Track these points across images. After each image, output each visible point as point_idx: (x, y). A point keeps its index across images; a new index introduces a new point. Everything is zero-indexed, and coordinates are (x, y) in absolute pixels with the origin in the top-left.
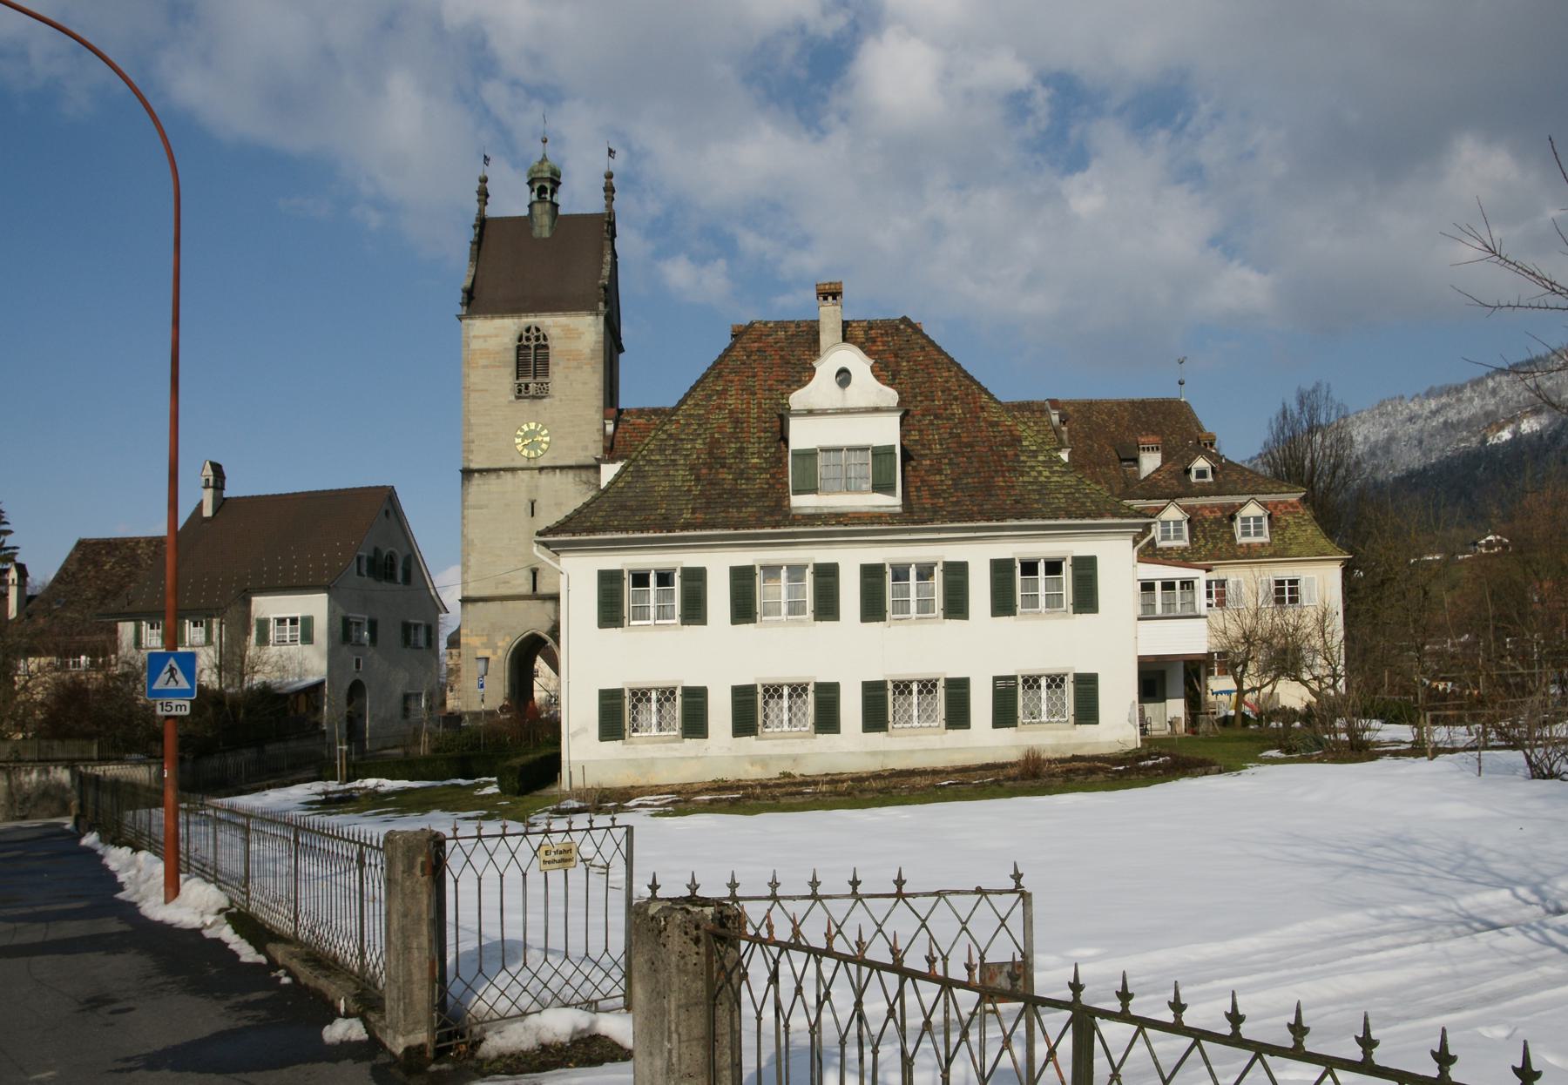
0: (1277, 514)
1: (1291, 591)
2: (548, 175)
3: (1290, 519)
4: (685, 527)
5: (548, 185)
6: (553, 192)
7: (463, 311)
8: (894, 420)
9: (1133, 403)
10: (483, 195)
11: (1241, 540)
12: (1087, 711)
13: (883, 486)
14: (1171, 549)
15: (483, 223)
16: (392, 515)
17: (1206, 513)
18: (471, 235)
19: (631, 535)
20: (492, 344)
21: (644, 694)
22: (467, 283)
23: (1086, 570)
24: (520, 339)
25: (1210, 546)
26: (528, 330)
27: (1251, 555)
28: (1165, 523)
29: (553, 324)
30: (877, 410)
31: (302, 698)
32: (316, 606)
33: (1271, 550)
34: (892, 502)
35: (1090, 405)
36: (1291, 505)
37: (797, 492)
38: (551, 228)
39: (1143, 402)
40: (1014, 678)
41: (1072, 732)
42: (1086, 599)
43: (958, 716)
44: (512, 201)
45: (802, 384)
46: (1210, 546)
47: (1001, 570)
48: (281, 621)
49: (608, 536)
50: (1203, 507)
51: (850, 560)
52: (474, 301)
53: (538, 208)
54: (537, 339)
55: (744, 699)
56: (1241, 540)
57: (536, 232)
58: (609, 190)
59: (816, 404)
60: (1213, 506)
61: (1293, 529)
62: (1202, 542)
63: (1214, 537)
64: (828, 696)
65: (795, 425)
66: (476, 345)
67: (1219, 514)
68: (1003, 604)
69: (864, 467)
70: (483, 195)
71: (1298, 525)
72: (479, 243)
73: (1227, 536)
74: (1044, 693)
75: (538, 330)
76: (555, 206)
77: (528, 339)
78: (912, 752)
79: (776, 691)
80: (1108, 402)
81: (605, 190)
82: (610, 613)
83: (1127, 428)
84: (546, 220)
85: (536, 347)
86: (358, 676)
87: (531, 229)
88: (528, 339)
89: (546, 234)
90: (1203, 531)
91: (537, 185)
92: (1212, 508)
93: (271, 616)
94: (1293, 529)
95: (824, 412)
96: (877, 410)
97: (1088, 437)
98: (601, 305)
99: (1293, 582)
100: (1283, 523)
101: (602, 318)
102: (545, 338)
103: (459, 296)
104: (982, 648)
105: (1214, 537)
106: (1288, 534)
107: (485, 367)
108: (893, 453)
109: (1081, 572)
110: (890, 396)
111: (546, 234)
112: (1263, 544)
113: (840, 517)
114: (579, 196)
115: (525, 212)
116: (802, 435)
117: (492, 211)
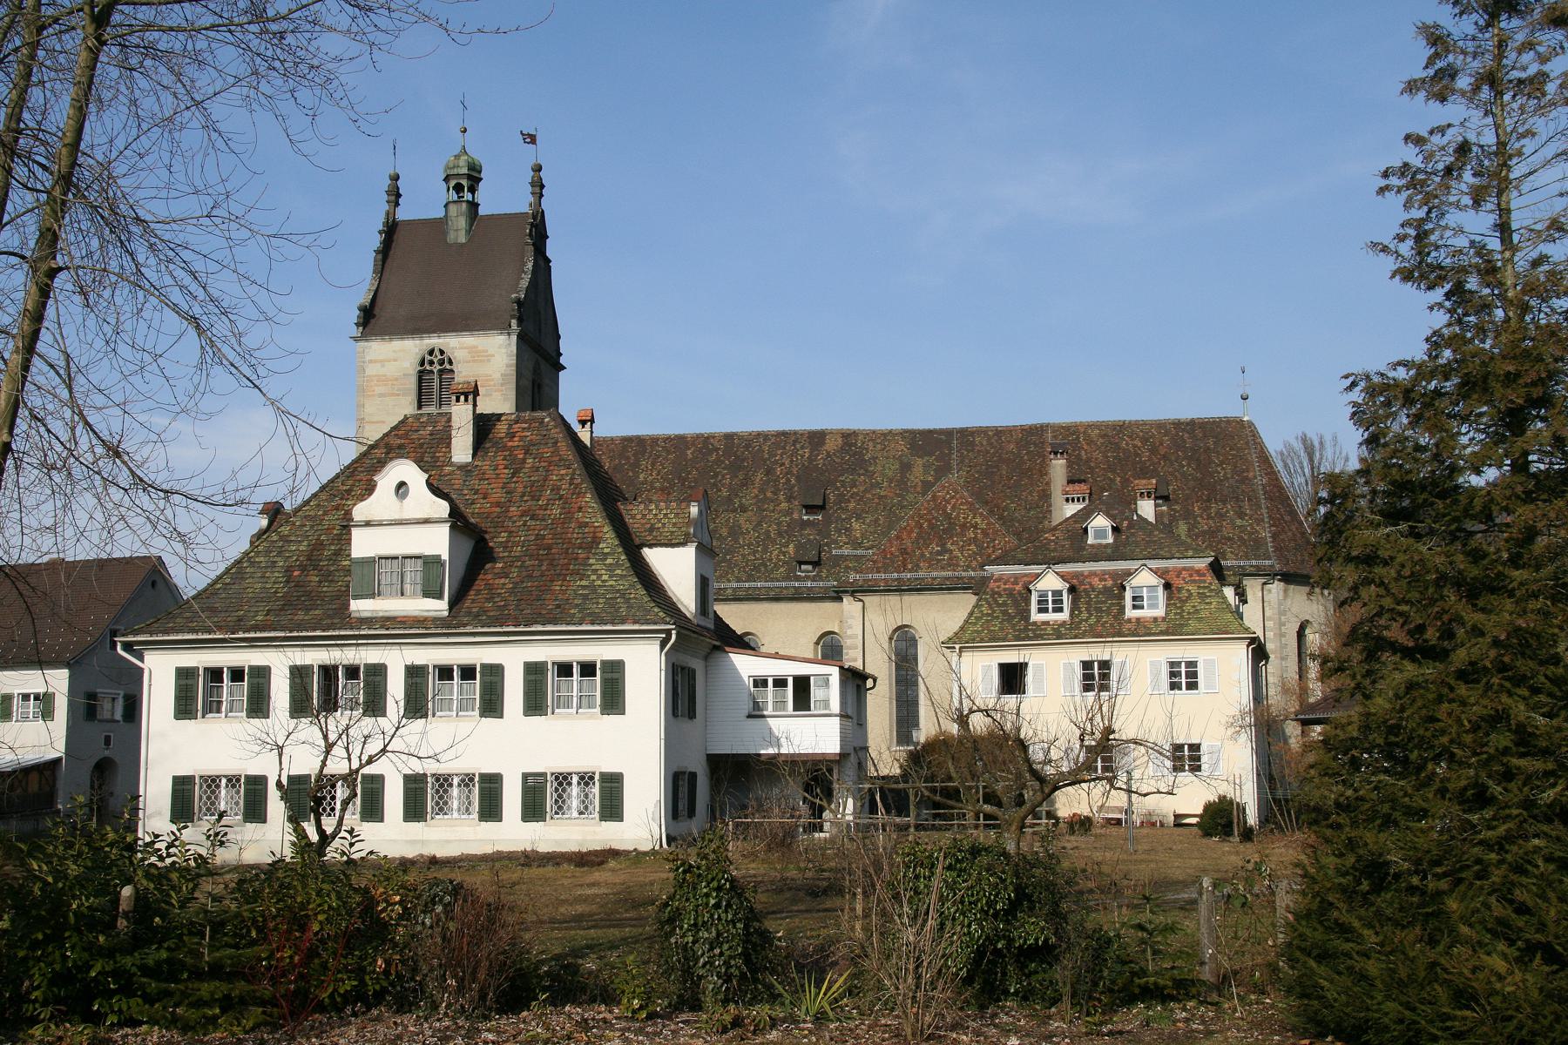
0: (1177, 582)
1: (1188, 675)
2: (465, 171)
3: (1193, 589)
4: (256, 628)
5: (464, 182)
6: (472, 190)
7: (356, 332)
8: (444, 530)
9: (1178, 424)
10: (395, 195)
11: (1036, 617)
12: (612, 808)
13: (432, 592)
14: (1047, 623)
15: (391, 230)
16: (160, 585)
17: (1096, 581)
18: (376, 241)
19: (201, 636)
20: (391, 370)
21: (565, 778)
22: (364, 298)
23: (613, 675)
24: (422, 363)
25: (1093, 620)
26: (431, 352)
27: (1142, 632)
28: (1043, 595)
29: (458, 345)
30: (426, 521)
31: (34, 776)
32: (58, 681)
33: (1163, 626)
34: (439, 607)
35: (1121, 428)
36: (1198, 572)
37: (356, 597)
38: (468, 231)
39: (1192, 422)
40: (544, 775)
41: (598, 829)
42: (613, 701)
43: (491, 809)
44: (426, 200)
45: (362, 498)
46: (1093, 620)
47: (534, 672)
48: (26, 697)
49: (180, 637)
50: (1093, 574)
51: (396, 660)
52: (370, 320)
53: (453, 209)
54: (441, 362)
55: (415, 787)
56: (1036, 617)
57: (451, 237)
58: (538, 186)
59: (376, 516)
60: (1104, 573)
61: (1195, 601)
62: (1085, 615)
63: (1099, 610)
64: (491, 786)
65: (356, 534)
66: (371, 370)
67: (1110, 583)
68: (535, 704)
69: (413, 572)
70: (395, 195)
71: (1202, 596)
72: (385, 252)
73: (1115, 610)
74: (455, 791)
75: (442, 352)
76: (474, 206)
77: (431, 363)
78: (448, 842)
79: (565, 778)
80: (1144, 423)
81: (533, 184)
82: (185, 708)
83: (1164, 457)
84: (462, 223)
85: (441, 372)
86: (107, 753)
87: (445, 233)
88: (431, 363)
89: (462, 239)
90: (1088, 603)
91: (452, 183)
92: (1102, 575)
93: (16, 692)
94: (1195, 601)
95: (380, 524)
96: (426, 521)
97: (1111, 469)
98: (514, 322)
99: (1192, 664)
100: (1184, 594)
101: (514, 338)
102: (451, 362)
103: (354, 315)
104: (514, 745)
105: (1099, 610)
106: (1188, 607)
107: (381, 395)
108: (443, 565)
109: (609, 676)
110: (442, 508)
111: (462, 239)
112: (1155, 619)
113: (388, 621)
114: (502, 196)
115: (442, 214)
116: (363, 544)
117: (402, 214)
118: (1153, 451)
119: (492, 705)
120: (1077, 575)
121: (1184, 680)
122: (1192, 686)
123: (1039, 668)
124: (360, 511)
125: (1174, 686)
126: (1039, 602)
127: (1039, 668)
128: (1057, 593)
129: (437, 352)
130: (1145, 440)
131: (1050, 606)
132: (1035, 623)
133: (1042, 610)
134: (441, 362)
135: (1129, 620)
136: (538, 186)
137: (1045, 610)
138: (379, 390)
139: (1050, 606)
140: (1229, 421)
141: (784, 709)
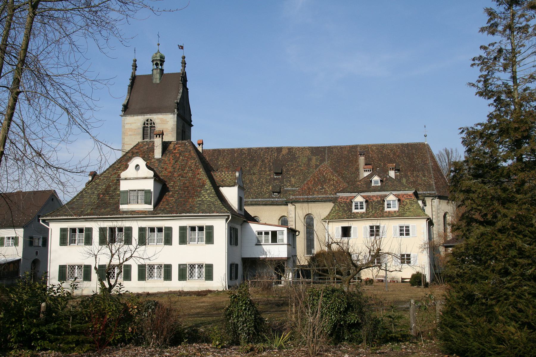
0: (402, 199)
1: (406, 231)
2: (159, 58)
3: (408, 201)
4: (87, 215)
5: (159, 62)
6: (161, 65)
7: (122, 113)
8: (152, 181)
9: (403, 145)
10: (135, 67)
11: (354, 211)
12: (209, 276)
13: (148, 202)
14: (358, 213)
15: (134, 78)
16: (55, 200)
17: (375, 199)
18: (129, 82)
19: (69, 217)
20: (134, 126)
21: (193, 266)
22: (124, 102)
23: (210, 231)
24: (144, 124)
25: (373, 212)
26: (147, 120)
27: (390, 216)
28: (356, 203)
29: (156, 118)
30: (146, 178)
31: (12, 265)
32: (20, 233)
33: (398, 214)
34: (150, 207)
35: (383, 146)
36: (410, 195)
37: (122, 204)
38: (160, 79)
39: (407, 144)
40: (186, 265)
41: (204, 283)
42: (210, 239)
43: (168, 276)
44: (146, 68)
45: (124, 170)
46: (373, 212)
47: (183, 229)
48: (9, 238)
49: (61, 218)
50: (374, 196)
51: (135, 226)
52: (127, 109)
53: (155, 71)
54: (151, 124)
55: (142, 269)
56: (354, 211)
57: (154, 81)
58: (184, 64)
59: (128, 176)
60: (377, 196)
61: (409, 205)
62: (371, 210)
63: (376, 208)
64: (168, 269)
65: (122, 182)
66: (127, 126)
67: (379, 199)
68: (183, 240)
69: (141, 195)
70: (135, 67)
71: (411, 204)
72: (132, 86)
73: (381, 208)
74: (156, 270)
75: (151, 120)
76: (162, 70)
77: (147, 124)
78: (153, 288)
79: (193, 266)
80: (391, 145)
81: (182, 63)
82: (63, 242)
83: (398, 156)
84: (158, 76)
85: (151, 127)
86: (36, 257)
87: (152, 80)
88: (147, 124)
89: (158, 82)
90: (372, 206)
91: (155, 63)
92: (377, 197)
93: (5, 236)
94: (409, 205)
95: (130, 179)
96: (146, 178)
97: (380, 160)
98: (176, 110)
99: (407, 227)
100: (405, 203)
101: (176, 115)
102: (154, 124)
103: (121, 108)
104: (176, 254)
105: (376, 208)
106: (406, 207)
107: (130, 135)
108: (151, 193)
109: (208, 231)
110: (151, 174)
111: (158, 82)
112: (395, 212)
113: (133, 212)
114: (172, 67)
115: (151, 73)
116: (124, 186)
117: (138, 73)
118: (394, 154)
119: (168, 241)
120: (368, 196)
121: (405, 232)
122: (408, 234)
123: (355, 228)
124: (123, 175)
125: (401, 234)
126: (355, 206)
127: (355, 228)
128: (361, 203)
129: (149, 120)
130: (391, 150)
131: (359, 207)
132: (354, 213)
133: (356, 208)
134: (151, 124)
135: (386, 212)
136: (184, 64)
137: (357, 209)
138: (130, 133)
139: (359, 207)
140: (420, 144)
141: (268, 242)
